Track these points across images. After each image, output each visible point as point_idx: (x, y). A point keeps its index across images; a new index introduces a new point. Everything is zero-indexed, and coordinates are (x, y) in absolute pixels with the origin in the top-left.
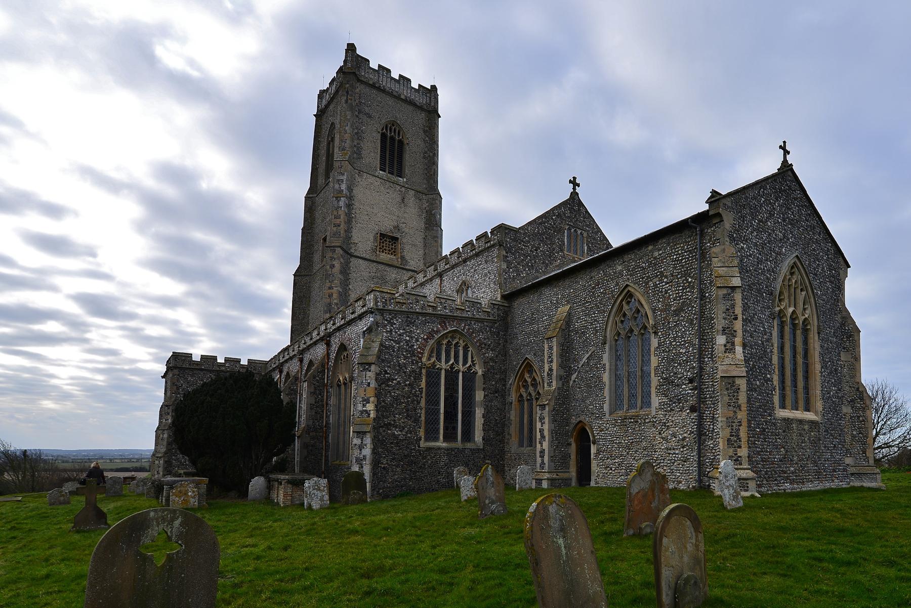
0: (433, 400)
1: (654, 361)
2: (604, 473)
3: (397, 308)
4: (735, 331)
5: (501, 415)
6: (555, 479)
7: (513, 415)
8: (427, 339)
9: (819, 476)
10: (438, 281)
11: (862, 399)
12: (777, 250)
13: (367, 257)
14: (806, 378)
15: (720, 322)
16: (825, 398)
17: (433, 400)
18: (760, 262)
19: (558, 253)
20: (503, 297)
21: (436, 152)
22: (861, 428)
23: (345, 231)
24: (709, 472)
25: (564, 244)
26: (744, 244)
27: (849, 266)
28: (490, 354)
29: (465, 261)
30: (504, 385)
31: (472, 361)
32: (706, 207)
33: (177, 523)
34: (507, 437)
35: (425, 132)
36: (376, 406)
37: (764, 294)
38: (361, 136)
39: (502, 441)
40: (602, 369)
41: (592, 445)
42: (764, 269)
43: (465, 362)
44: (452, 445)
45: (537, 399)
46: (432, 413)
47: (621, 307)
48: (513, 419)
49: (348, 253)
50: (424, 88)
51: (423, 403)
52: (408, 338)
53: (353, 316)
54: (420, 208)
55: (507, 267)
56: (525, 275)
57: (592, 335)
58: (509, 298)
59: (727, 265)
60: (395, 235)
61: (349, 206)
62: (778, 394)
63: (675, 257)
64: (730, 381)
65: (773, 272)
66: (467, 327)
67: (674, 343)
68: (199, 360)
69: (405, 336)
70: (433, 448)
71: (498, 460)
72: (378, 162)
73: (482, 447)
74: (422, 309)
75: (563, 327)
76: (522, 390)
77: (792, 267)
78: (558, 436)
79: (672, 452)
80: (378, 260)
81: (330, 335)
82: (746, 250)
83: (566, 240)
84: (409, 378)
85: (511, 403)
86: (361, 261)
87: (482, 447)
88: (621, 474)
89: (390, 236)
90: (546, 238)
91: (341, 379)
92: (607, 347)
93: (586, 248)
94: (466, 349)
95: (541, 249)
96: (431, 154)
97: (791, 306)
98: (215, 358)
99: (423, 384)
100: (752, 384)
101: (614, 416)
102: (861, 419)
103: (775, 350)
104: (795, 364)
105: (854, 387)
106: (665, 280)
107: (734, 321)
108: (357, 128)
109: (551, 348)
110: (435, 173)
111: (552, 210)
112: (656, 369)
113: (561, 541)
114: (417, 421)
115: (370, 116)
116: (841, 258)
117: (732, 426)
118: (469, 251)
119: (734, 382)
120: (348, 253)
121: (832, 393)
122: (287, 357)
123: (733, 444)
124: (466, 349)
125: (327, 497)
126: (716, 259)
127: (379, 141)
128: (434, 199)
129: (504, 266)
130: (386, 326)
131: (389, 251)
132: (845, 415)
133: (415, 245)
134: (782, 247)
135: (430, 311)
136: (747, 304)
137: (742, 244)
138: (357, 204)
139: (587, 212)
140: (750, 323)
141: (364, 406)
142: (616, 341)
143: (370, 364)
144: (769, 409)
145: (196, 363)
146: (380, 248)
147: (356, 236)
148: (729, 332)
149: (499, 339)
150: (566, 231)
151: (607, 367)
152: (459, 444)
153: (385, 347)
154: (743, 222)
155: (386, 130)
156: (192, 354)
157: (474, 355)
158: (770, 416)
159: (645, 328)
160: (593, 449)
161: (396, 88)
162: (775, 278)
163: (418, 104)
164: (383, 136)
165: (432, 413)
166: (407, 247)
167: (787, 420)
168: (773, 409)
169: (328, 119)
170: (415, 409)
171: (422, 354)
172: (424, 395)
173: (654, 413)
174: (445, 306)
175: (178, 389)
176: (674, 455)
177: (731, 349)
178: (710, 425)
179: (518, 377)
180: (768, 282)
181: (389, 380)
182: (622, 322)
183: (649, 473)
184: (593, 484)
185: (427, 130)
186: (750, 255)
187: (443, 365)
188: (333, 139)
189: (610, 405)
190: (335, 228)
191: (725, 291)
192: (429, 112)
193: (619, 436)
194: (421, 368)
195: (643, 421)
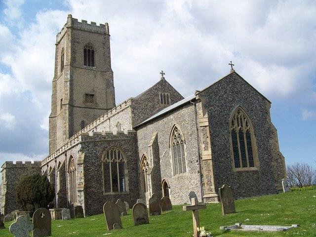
0: (107, 177)
10: (108, 121)
16: (261, 160)
17: (107, 177)
20: (133, 128)
28: (130, 154)
29: (118, 113)
31: (122, 157)
35: (104, 44)
36: (85, 180)
43: (119, 158)
44: (117, 193)
45: (146, 172)
46: (107, 181)
49: (72, 106)
51: (103, 177)
53: (74, 144)
81: (66, 151)
99: (102, 169)
101: (175, 177)
114: (101, 184)
115: (79, 43)
120: (72, 106)
122: (50, 160)
134: (232, 104)
143: (81, 164)
145: (15, 165)
152: (119, 193)
160: (169, 190)
161: (90, 28)
164: (85, 50)
165: (107, 181)
167: (240, 173)
169: (61, 46)
172: (103, 174)
173: (187, 175)
187: (110, 161)
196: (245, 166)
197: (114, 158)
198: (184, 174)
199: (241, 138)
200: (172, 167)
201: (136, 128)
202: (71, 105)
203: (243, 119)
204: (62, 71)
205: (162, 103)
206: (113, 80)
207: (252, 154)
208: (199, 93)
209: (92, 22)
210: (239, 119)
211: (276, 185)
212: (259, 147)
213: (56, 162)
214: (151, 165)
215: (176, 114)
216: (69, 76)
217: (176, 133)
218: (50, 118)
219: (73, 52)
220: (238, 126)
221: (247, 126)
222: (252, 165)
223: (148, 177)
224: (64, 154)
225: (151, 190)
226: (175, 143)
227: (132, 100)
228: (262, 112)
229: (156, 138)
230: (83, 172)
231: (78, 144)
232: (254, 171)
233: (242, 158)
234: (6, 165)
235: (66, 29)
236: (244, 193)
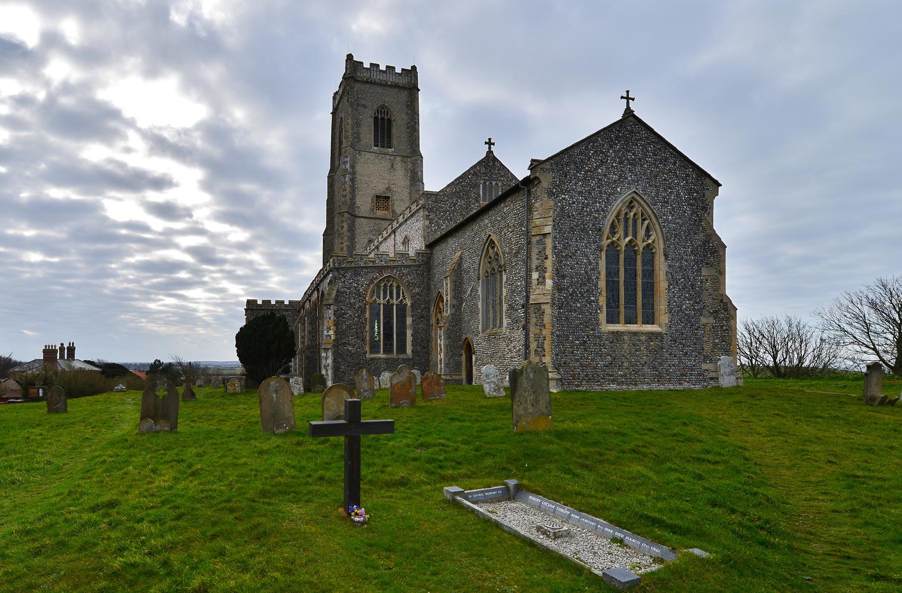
3: (348, 266)
4: (546, 268)
6: (449, 380)
9: (659, 378)
11: (726, 310)
15: (535, 262)
19: (474, 204)
21: (417, 121)
22: (724, 336)
23: (351, 199)
25: (480, 196)
26: (565, 195)
28: (417, 290)
29: (406, 221)
30: (429, 312)
31: (403, 296)
32: (528, 173)
33: (166, 385)
34: (431, 350)
35: (407, 106)
36: (335, 332)
37: (590, 232)
43: (398, 297)
44: (390, 356)
49: (353, 215)
54: (405, 169)
58: (431, 246)
59: (543, 216)
60: (387, 195)
61: (353, 180)
64: (537, 306)
65: (603, 211)
66: (398, 272)
71: (424, 366)
73: (411, 357)
74: (365, 264)
75: (456, 268)
77: (631, 202)
78: (452, 349)
80: (375, 216)
83: (481, 192)
86: (363, 220)
87: (411, 357)
90: (463, 194)
94: (398, 288)
96: (413, 124)
98: (270, 301)
99: (367, 315)
102: (724, 328)
105: (717, 299)
107: (545, 260)
108: (356, 119)
109: (447, 284)
110: (417, 138)
111: (468, 171)
113: (274, 395)
114: (363, 340)
115: (365, 106)
117: (539, 340)
119: (540, 307)
120: (353, 215)
123: (539, 354)
124: (398, 288)
125: (302, 389)
126: (536, 212)
127: (373, 124)
128: (416, 160)
129: (427, 223)
130: (341, 278)
135: (371, 265)
138: (358, 177)
139: (501, 164)
141: (328, 332)
142: (487, 277)
143: (330, 305)
147: (359, 201)
148: (542, 269)
151: (481, 297)
155: (378, 113)
158: (593, 330)
161: (383, 77)
163: (401, 85)
164: (376, 119)
166: (397, 203)
167: (617, 335)
168: (598, 325)
169: (341, 114)
170: (362, 332)
171: (366, 295)
172: (368, 323)
177: (543, 282)
180: (596, 221)
181: (344, 314)
182: (489, 262)
183: (406, 373)
184: (474, 384)
185: (409, 105)
189: (483, 325)
191: (538, 238)
192: (410, 89)
194: (365, 305)
196: (629, 321)
197: (388, 297)
199: (630, 261)
200: (480, 315)
203: (640, 221)
207: (652, 296)
210: (631, 222)
211: (704, 366)
217: (491, 251)
220: (626, 235)
221: (648, 235)
222: (649, 319)
223: (439, 332)
225: (442, 354)
226: (489, 271)
228: (692, 205)
232: (652, 333)
233: (626, 302)
236: (621, 376)
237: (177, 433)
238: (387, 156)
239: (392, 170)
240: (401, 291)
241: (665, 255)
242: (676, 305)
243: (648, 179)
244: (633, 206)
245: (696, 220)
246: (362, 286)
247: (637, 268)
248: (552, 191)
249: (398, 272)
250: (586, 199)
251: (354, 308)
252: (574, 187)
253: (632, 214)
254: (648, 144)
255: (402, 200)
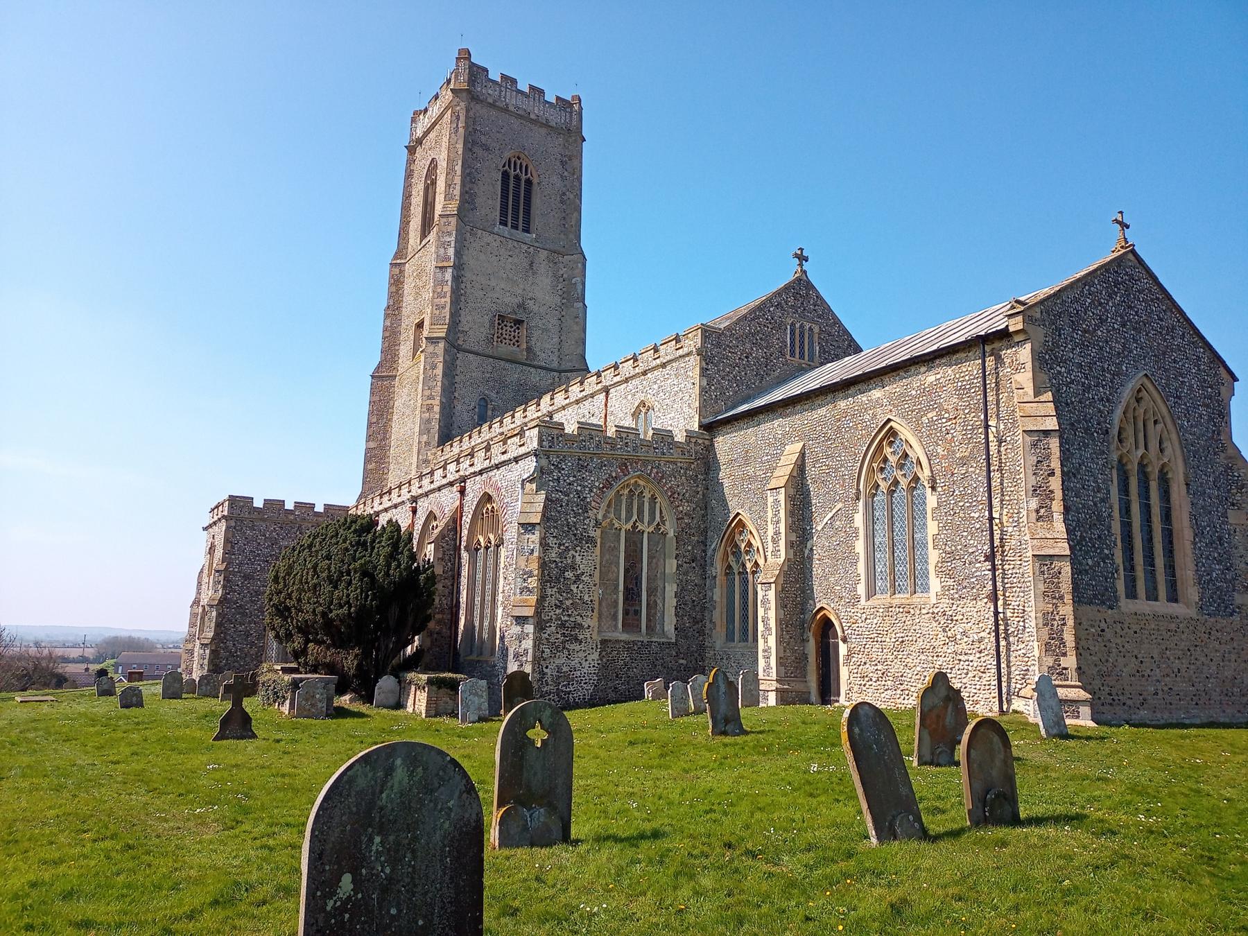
1: (932, 527)
2: (860, 685)
4: (1052, 492)
5: (700, 593)
7: (718, 594)
8: (603, 488)
12: (1113, 369)
13: (480, 350)
14: (1169, 552)
16: (1203, 582)
18: (1087, 389)
20: (700, 427)
24: (1020, 689)
26: (1061, 368)
27: (1235, 379)
28: (685, 508)
29: (645, 373)
30: (704, 551)
31: (661, 517)
37: (1095, 434)
38: (474, 177)
39: (701, 632)
40: (854, 535)
41: (841, 643)
42: (1093, 398)
45: (754, 573)
47: (880, 447)
48: (718, 600)
50: (563, 100)
52: (579, 488)
55: (708, 384)
56: (731, 393)
57: (838, 486)
62: (1122, 577)
63: (960, 384)
66: (655, 470)
67: (961, 504)
68: (262, 507)
69: (575, 484)
70: (610, 641)
72: (498, 215)
73: (674, 640)
75: (795, 474)
76: (731, 558)
77: (1139, 391)
79: (963, 658)
81: (463, 479)
82: (1065, 375)
83: (788, 339)
84: (580, 542)
85: (715, 577)
87: (674, 640)
88: (886, 687)
89: (510, 318)
91: (482, 540)
92: (861, 504)
93: (818, 348)
94: (653, 498)
95: (754, 355)
97: (1140, 446)
100: (1081, 564)
103: (1116, 514)
104: (1151, 531)
106: (947, 415)
111: (770, 300)
112: (935, 537)
116: (1222, 369)
118: (650, 359)
121: (1214, 575)
124: (653, 498)
127: (499, 183)
130: (552, 473)
131: (511, 340)
132: (1239, 608)
133: (547, 330)
136: (1069, 451)
137: (1058, 368)
138: (468, 275)
139: (819, 296)
140: (1075, 477)
143: (533, 525)
144: (1109, 600)
146: (498, 337)
147: (466, 320)
149: (697, 486)
150: (789, 327)
153: (551, 501)
154: (1060, 335)
155: (509, 166)
156: (252, 499)
157: (663, 509)
159: (916, 479)
160: (843, 649)
161: (524, 104)
162: (1112, 410)
164: (505, 175)
168: (1117, 599)
174: (627, 443)
175: (233, 547)
176: (967, 663)
178: (1019, 622)
179: (724, 540)
180: (1101, 416)
186: (1072, 382)
188: (434, 183)
190: (438, 312)
193: (881, 632)
195: (918, 612)
197: (635, 517)
198: (918, 599)
201: (711, 428)
202: (454, 343)
203: (1150, 424)
204: (424, 235)
205: (793, 354)
206: (584, 284)
208: (1027, 311)
209: (504, 77)
212: (1198, 533)
213: (414, 511)
214: (775, 552)
215: (895, 387)
216: (451, 252)
218: (373, 377)
219: (469, 177)
224: (455, 488)
227: (707, 332)
228: (1207, 406)
229: (800, 466)
230: (536, 554)
231: (527, 455)
234: (231, 507)
235: (448, 96)
237: (577, 842)
238: (523, 246)
239: (530, 273)
240: (658, 506)
241: (1187, 484)
242: (1204, 571)
243: (1155, 356)
244: (1142, 398)
245: (1214, 431)
246: (591, 491)
247: (1152, 502)
248: (1044, 357)
249: (655, 470)
250: (1087, 378)
251: (575, 535)
252: (1071, 355)
253: (1142, 411)
254: (1152, 300)
255: (546, 330)
